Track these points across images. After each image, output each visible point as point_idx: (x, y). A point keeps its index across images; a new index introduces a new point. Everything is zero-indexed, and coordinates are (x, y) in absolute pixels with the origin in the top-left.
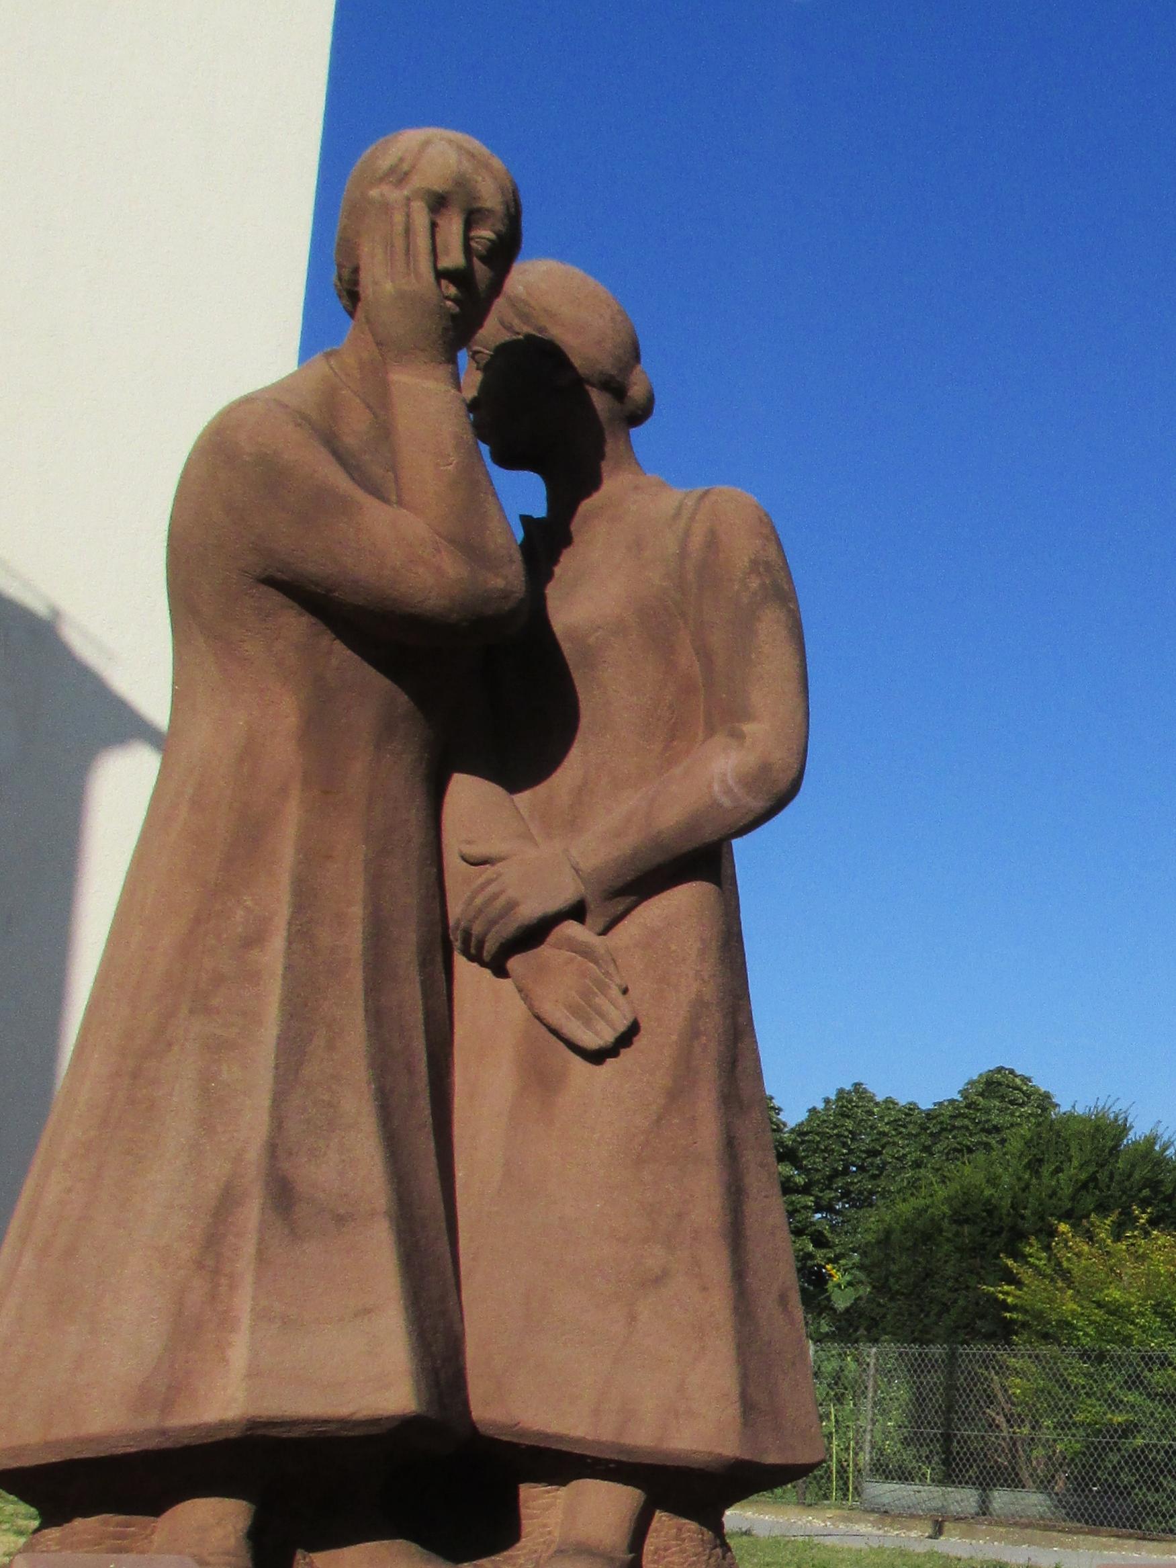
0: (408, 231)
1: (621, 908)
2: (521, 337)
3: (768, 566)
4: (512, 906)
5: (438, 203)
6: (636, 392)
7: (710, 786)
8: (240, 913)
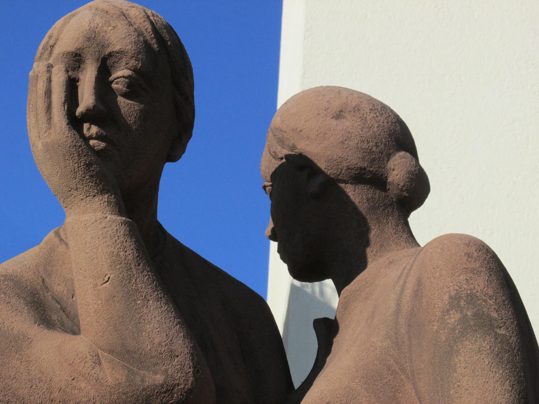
0: (48, 93)
2: (284, 160)
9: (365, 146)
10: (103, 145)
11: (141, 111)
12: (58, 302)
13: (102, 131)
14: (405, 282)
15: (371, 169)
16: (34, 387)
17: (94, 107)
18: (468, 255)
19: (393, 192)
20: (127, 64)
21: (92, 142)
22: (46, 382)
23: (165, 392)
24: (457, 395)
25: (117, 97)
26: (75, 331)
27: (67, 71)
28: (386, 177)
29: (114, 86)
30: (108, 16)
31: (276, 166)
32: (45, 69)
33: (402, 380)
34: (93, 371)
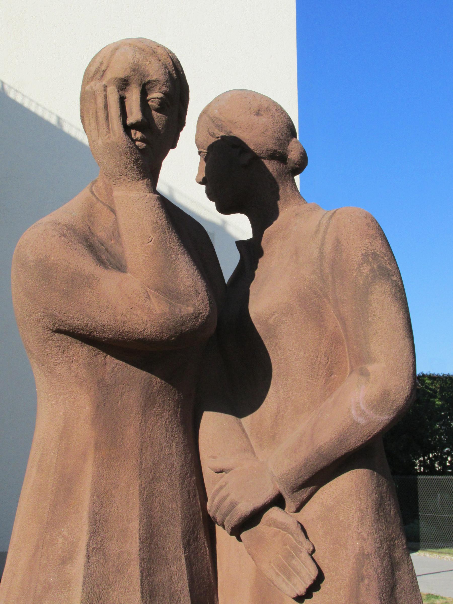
0: (106, 106)
1: (305, 495)
2: (220, 139)
3: (375, 255)
4: (233, 505)
5: (124, 84)
6: (293, 155)
7: (349, 411)
8: (61, 540)
9: (276, 135)
10: (144, 145)
11: (166, 121)
12: (102, 245)
13: (144, 136)
14: (324, 238)
15: (280, 151)
16: (103, 311)
17: (142, 120)
18: (367, 224)
19: (290, 165)
20: (160, 89)
21: (137, 143)
22: (112, 309)
23: (194, 319)
24: (373, 321)
25: (151, 111)
26: (120, 267)
27: (119, 92)
28: (287, 156)
29: (150, 103)
30: (144, 53)
31: (213, 141)
32: (103, 89)
33: (324, 302)
34: (146, 304)
